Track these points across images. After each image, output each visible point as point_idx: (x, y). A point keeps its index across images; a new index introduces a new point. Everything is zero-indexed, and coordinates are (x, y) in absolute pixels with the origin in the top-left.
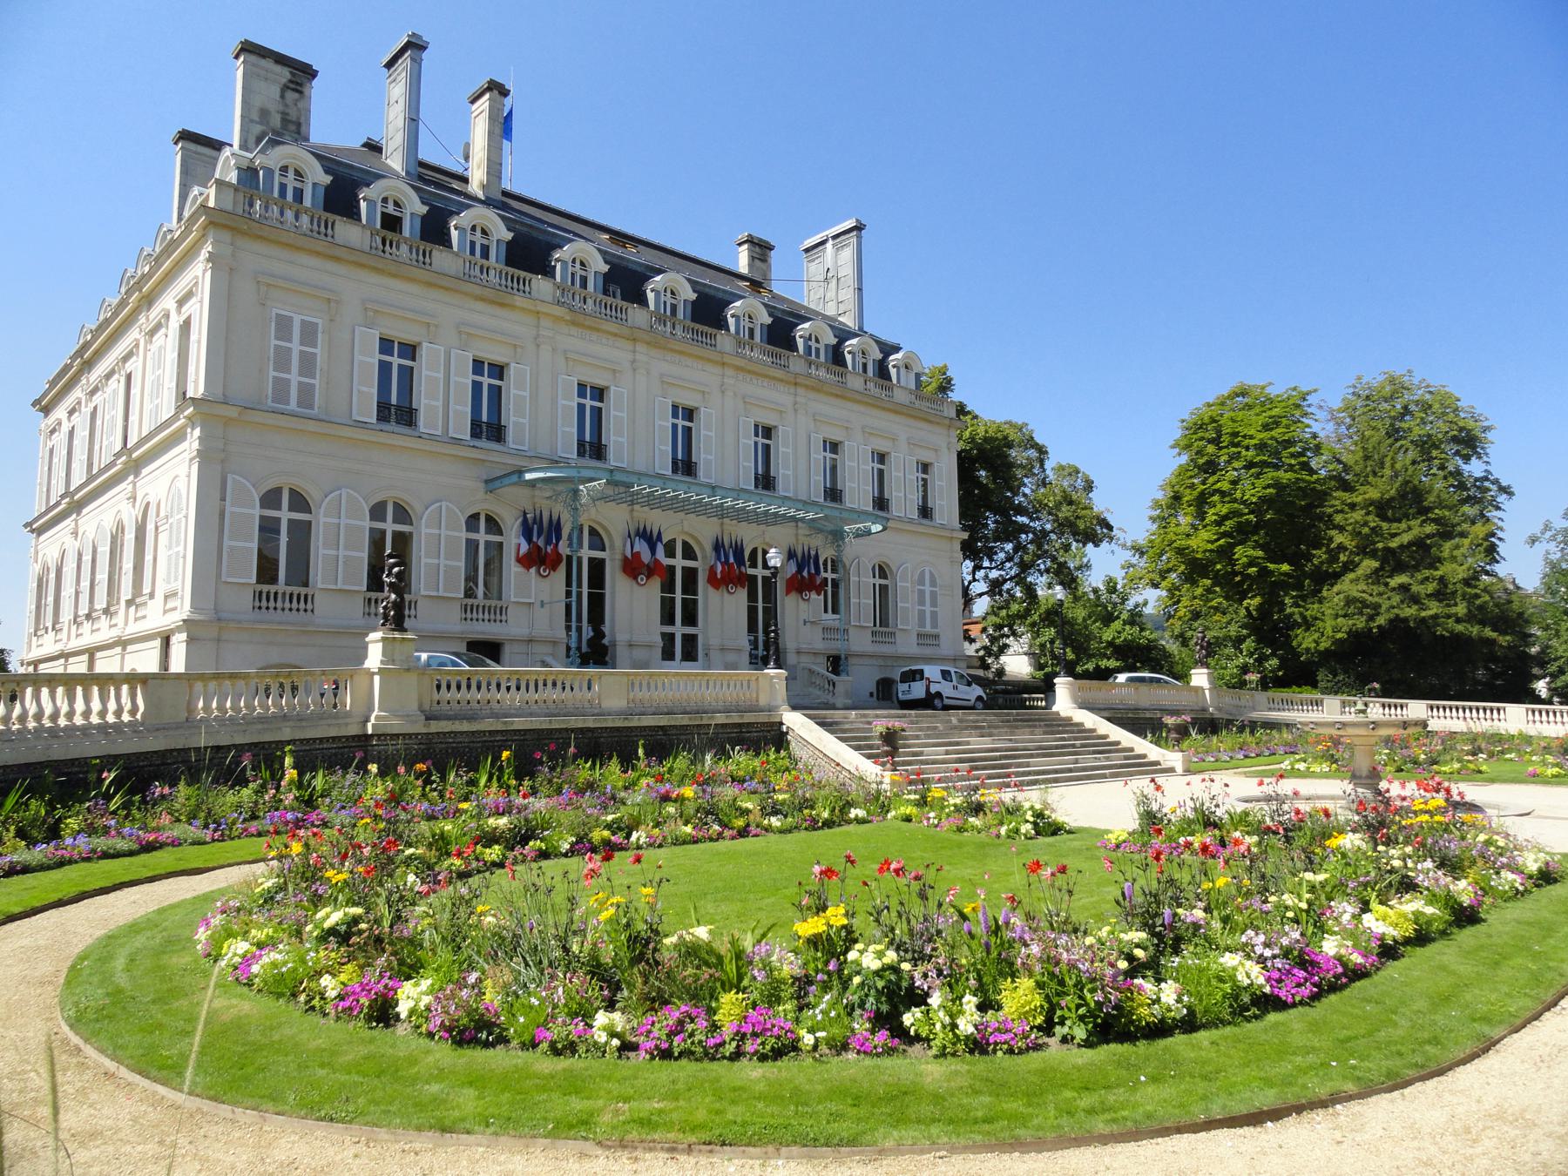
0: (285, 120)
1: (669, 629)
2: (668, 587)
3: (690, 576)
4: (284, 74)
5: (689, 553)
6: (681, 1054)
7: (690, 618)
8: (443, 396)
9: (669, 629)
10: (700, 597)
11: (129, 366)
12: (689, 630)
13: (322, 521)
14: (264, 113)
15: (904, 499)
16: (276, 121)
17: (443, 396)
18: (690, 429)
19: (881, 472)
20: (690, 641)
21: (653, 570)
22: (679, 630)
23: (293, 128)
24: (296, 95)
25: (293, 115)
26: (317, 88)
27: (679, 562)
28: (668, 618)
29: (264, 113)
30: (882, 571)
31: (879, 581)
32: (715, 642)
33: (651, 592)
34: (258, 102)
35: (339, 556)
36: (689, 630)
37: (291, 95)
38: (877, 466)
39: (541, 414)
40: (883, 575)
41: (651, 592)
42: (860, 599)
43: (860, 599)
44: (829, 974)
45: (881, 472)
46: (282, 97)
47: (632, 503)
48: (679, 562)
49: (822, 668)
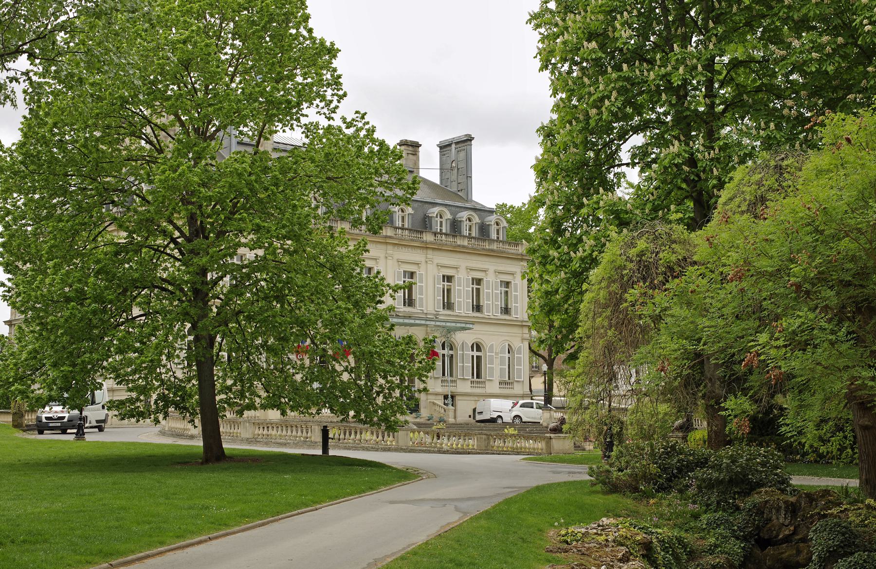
6: (450, 145)
30: (478, 347)
31: (475, 354)
40: (479, 349)
49: (440, 401)
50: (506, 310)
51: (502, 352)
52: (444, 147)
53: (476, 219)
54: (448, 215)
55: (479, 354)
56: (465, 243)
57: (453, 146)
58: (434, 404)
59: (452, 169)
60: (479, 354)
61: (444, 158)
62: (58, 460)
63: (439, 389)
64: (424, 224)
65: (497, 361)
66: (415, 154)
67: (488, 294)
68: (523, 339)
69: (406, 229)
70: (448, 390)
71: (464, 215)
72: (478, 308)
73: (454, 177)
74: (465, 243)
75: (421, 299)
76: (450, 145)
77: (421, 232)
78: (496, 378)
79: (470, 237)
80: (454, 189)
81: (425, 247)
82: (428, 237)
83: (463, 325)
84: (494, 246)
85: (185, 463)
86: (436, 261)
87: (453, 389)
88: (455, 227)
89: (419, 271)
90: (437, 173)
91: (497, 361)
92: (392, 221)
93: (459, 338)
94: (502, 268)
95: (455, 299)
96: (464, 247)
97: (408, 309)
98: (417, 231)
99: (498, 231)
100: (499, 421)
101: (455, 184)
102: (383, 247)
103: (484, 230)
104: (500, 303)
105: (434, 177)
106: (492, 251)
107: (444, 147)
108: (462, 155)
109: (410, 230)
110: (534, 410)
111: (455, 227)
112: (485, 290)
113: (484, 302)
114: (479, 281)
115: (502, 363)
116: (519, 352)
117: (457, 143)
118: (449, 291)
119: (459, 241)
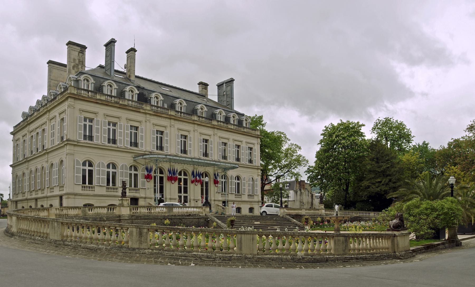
0: (79, 61)
1: (180, 194)
2: (202, 186)
3: (185, 180)
4: (79, 48)
5: (185, 174)
6: (223, 84)
7: (186, 191)
8: (123, 140)
9: (180, 194)
10: (188, 186)
11: (44, 127)
12: (185, 195)
13: (95, 169)
14: (74, 60)
15: (244, 160)
16: (77, 62)
17: (123, 140)
18: (185, 141)
19: (238, 151)
20: (186, 198)
21: (175, 179)
22: (183, 195)
23: (81, 63)
24: (82, 54)
25: (81, 60)
26: (87, 51)
27: (183, 177)
28: (180, 191)
29: (74, 60)
30: (238, 178)
31: (237, 181)
32: (192, 198)
33: (175, 185)
34: (72, 57)
35: (99, 177)
36: (185, 195)
37: (81, 54)
38: (237, 149)
39: (147, 144)
40: (238, 179)
41: (175, 185)
42: (232, 187)
43: (232, 187)
44: (274, 250)
45: (238, 151)
46: (79, 55)
47: (170, 162)
48: (183, 177)
49: (221, 204)
50: (251, 161)
51: (249, 180)
52: (220, 86)
53: (237, 117)
54: (224, 114)
55: (238, 181)
56: (232, 127)
57: (224, 84)
58: (218, 205)
59: (224, 95)
60: (238, 181)
61: (220, 91)
62: (373, 194)
63: (220, 198)
64: (212, 117)
65: (247, 185)
66: (206, 89)
67: (243, 153)
68: (258, 175)
69: (204, 118)
70: (223, 199)
71: (232, 115)
72: (238, 159)
73: (225, 99)
74: (232, 127)
75: (211, 153)
76: (223, 84)
77: (211, 120)
78: (247, 193)
79: (234, 125)
80: (225, 105)
81: (213, 127)
82: (215, 123)
83: (234, 165)
84: (246, 130)
85: (365, 259)
86: (218, 135)
87: (227, 198)
88: (227, 120)
89: (211, 139)
90: (217, 97)
91: (247, 185)
92: (197, 114)
93: (231, 173)
94: (249, 141)
95: (228, 155)
96: (231, 129)
97: (205, 158)
98: (209, 119)
99: (246, 124)
100: (264, 214)
101: (225, 102)
102: (192, 125)
103: (240, 123)
104: (248, 158)
105: (216, 99)
106: (245, 132)
107: (220, 86)
108: (229, 88)
109: (206, 118)
110: (273, 208)
111: (227, 120)
112: (241, 151)
113: (241, 157)
114: (238, 146)
115: (249, 186)
116: (257, 181)
117: (226, 83)
118: (225, 150)
119: (230, 126)
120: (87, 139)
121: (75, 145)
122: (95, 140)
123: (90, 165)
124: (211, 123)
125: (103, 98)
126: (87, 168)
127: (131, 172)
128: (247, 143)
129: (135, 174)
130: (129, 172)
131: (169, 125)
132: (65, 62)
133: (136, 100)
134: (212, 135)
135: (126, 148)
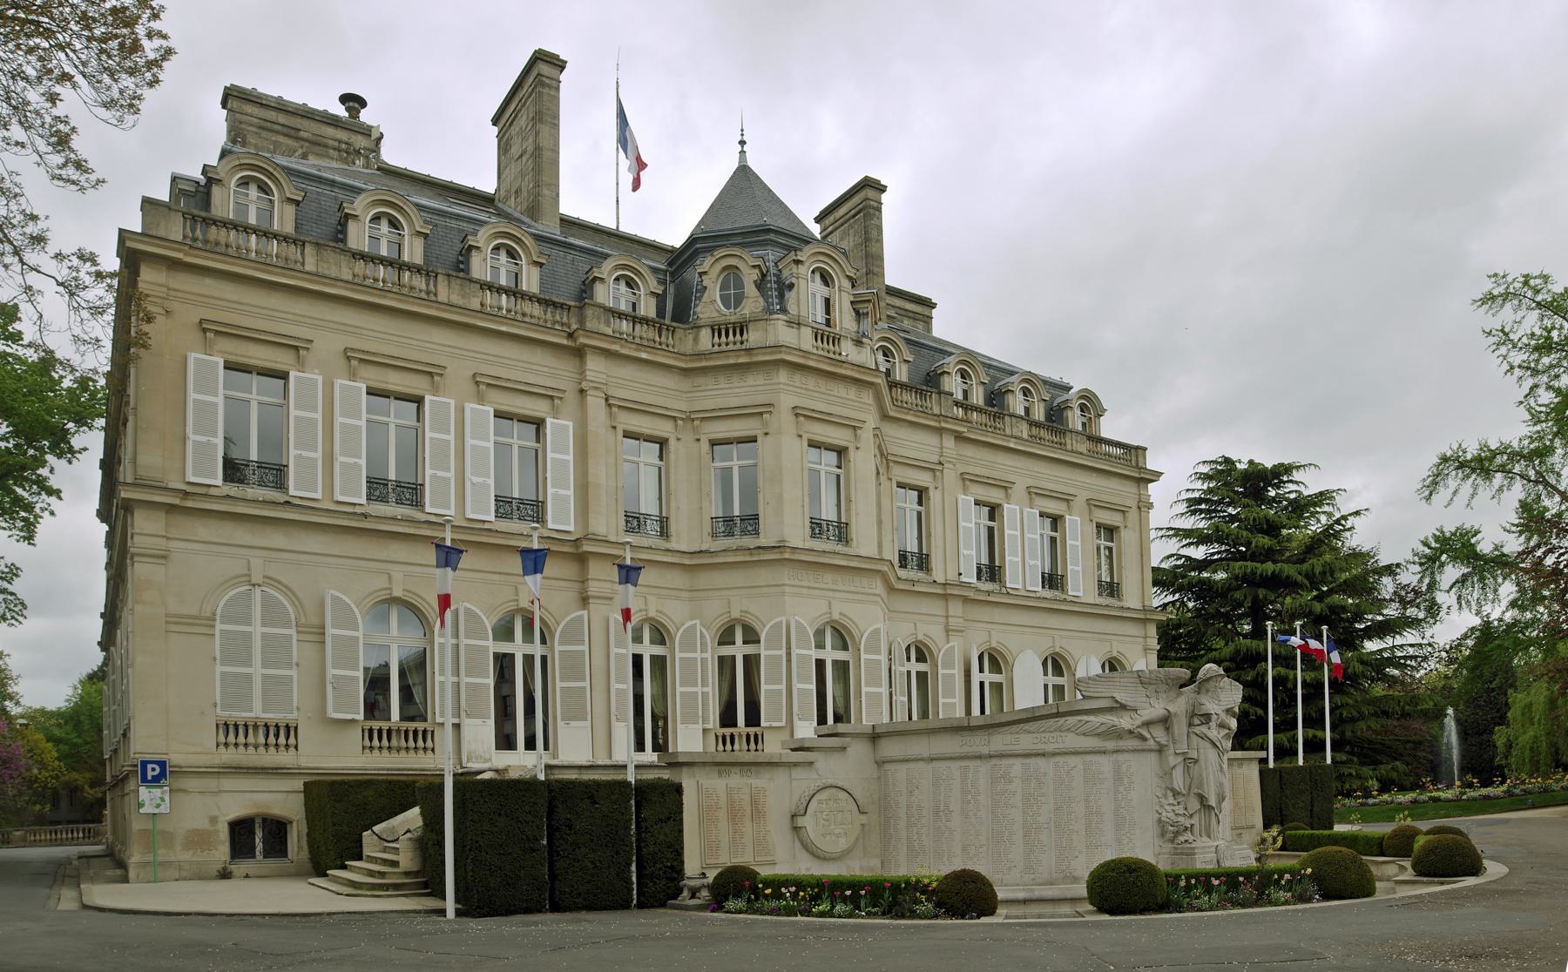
31: (915, 667)
40: (921, 658)
68: (1146, 649)
104: (1039, 564)
120: (392, 497)
121: (170, 509)
122: (549, 517)
123: (751, 637)
124: (430, 297)
125: (345, 269)
126: (739, 650)
127: (821, 655)
128: (1092, 504)
129: (746, 658)
130: (815, 654)
131: (1134, 504)
132: (488, 184)
133: (1042, 419)
134: (571, 397)
135: (204, 492)
